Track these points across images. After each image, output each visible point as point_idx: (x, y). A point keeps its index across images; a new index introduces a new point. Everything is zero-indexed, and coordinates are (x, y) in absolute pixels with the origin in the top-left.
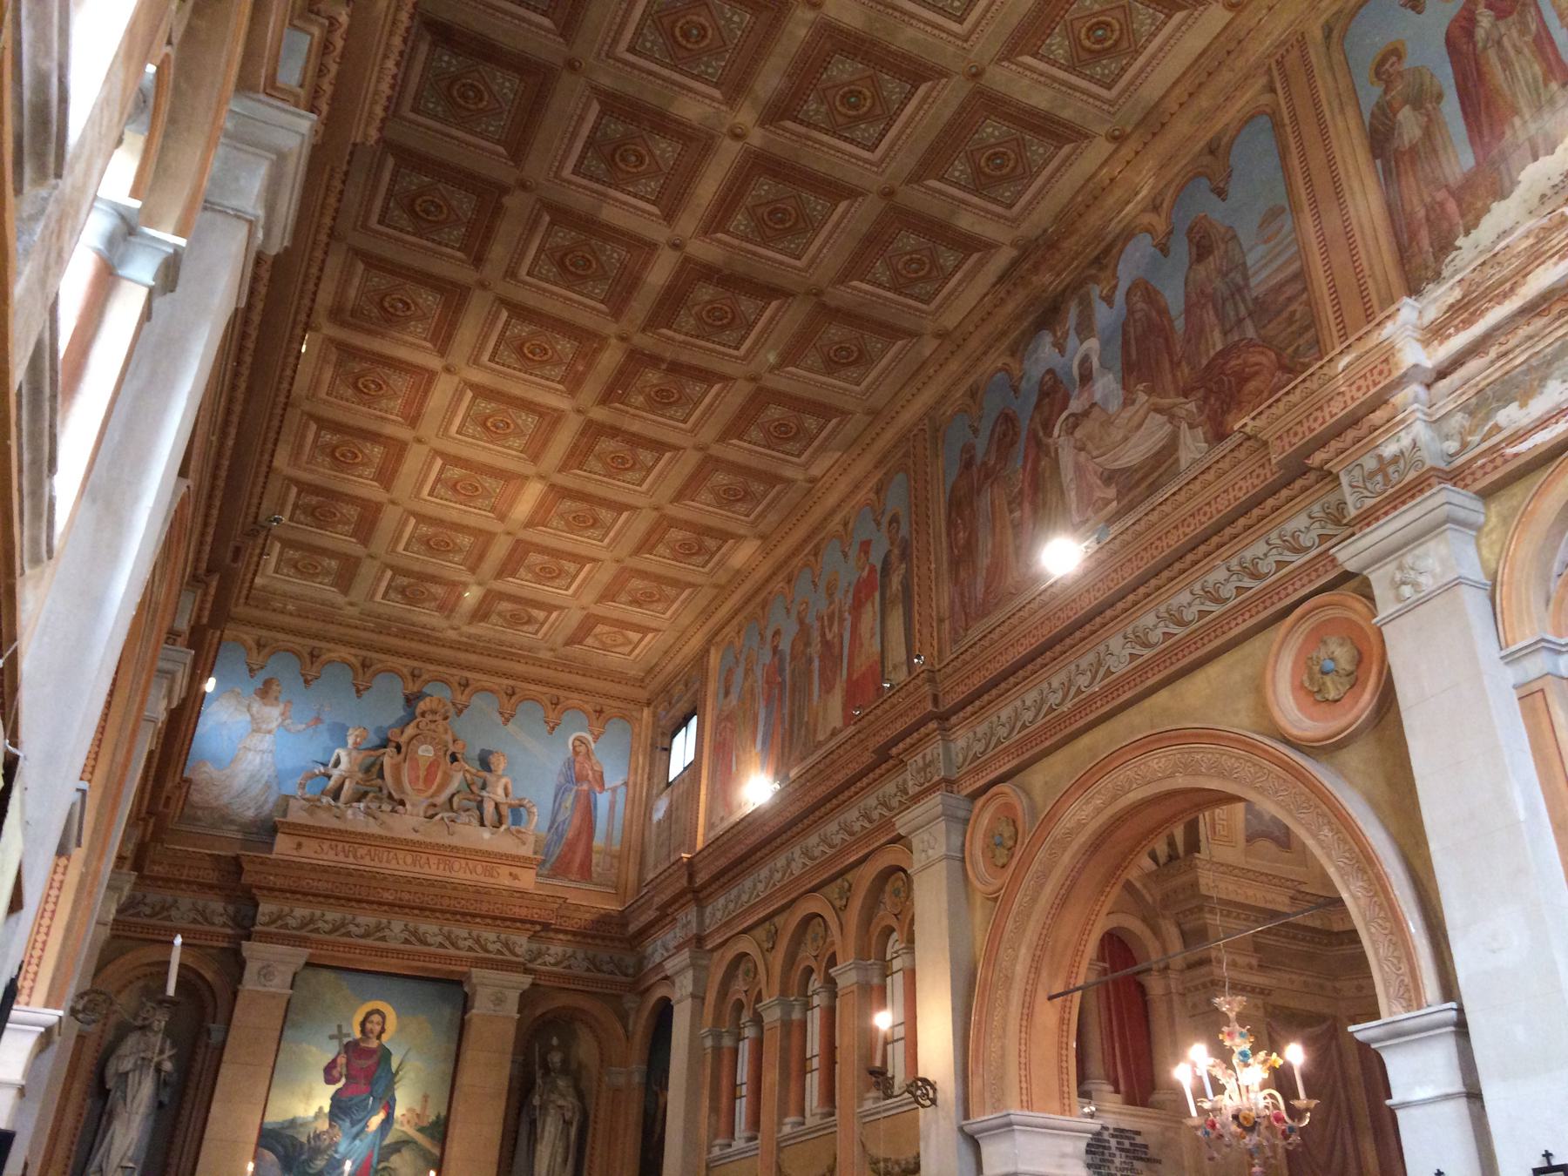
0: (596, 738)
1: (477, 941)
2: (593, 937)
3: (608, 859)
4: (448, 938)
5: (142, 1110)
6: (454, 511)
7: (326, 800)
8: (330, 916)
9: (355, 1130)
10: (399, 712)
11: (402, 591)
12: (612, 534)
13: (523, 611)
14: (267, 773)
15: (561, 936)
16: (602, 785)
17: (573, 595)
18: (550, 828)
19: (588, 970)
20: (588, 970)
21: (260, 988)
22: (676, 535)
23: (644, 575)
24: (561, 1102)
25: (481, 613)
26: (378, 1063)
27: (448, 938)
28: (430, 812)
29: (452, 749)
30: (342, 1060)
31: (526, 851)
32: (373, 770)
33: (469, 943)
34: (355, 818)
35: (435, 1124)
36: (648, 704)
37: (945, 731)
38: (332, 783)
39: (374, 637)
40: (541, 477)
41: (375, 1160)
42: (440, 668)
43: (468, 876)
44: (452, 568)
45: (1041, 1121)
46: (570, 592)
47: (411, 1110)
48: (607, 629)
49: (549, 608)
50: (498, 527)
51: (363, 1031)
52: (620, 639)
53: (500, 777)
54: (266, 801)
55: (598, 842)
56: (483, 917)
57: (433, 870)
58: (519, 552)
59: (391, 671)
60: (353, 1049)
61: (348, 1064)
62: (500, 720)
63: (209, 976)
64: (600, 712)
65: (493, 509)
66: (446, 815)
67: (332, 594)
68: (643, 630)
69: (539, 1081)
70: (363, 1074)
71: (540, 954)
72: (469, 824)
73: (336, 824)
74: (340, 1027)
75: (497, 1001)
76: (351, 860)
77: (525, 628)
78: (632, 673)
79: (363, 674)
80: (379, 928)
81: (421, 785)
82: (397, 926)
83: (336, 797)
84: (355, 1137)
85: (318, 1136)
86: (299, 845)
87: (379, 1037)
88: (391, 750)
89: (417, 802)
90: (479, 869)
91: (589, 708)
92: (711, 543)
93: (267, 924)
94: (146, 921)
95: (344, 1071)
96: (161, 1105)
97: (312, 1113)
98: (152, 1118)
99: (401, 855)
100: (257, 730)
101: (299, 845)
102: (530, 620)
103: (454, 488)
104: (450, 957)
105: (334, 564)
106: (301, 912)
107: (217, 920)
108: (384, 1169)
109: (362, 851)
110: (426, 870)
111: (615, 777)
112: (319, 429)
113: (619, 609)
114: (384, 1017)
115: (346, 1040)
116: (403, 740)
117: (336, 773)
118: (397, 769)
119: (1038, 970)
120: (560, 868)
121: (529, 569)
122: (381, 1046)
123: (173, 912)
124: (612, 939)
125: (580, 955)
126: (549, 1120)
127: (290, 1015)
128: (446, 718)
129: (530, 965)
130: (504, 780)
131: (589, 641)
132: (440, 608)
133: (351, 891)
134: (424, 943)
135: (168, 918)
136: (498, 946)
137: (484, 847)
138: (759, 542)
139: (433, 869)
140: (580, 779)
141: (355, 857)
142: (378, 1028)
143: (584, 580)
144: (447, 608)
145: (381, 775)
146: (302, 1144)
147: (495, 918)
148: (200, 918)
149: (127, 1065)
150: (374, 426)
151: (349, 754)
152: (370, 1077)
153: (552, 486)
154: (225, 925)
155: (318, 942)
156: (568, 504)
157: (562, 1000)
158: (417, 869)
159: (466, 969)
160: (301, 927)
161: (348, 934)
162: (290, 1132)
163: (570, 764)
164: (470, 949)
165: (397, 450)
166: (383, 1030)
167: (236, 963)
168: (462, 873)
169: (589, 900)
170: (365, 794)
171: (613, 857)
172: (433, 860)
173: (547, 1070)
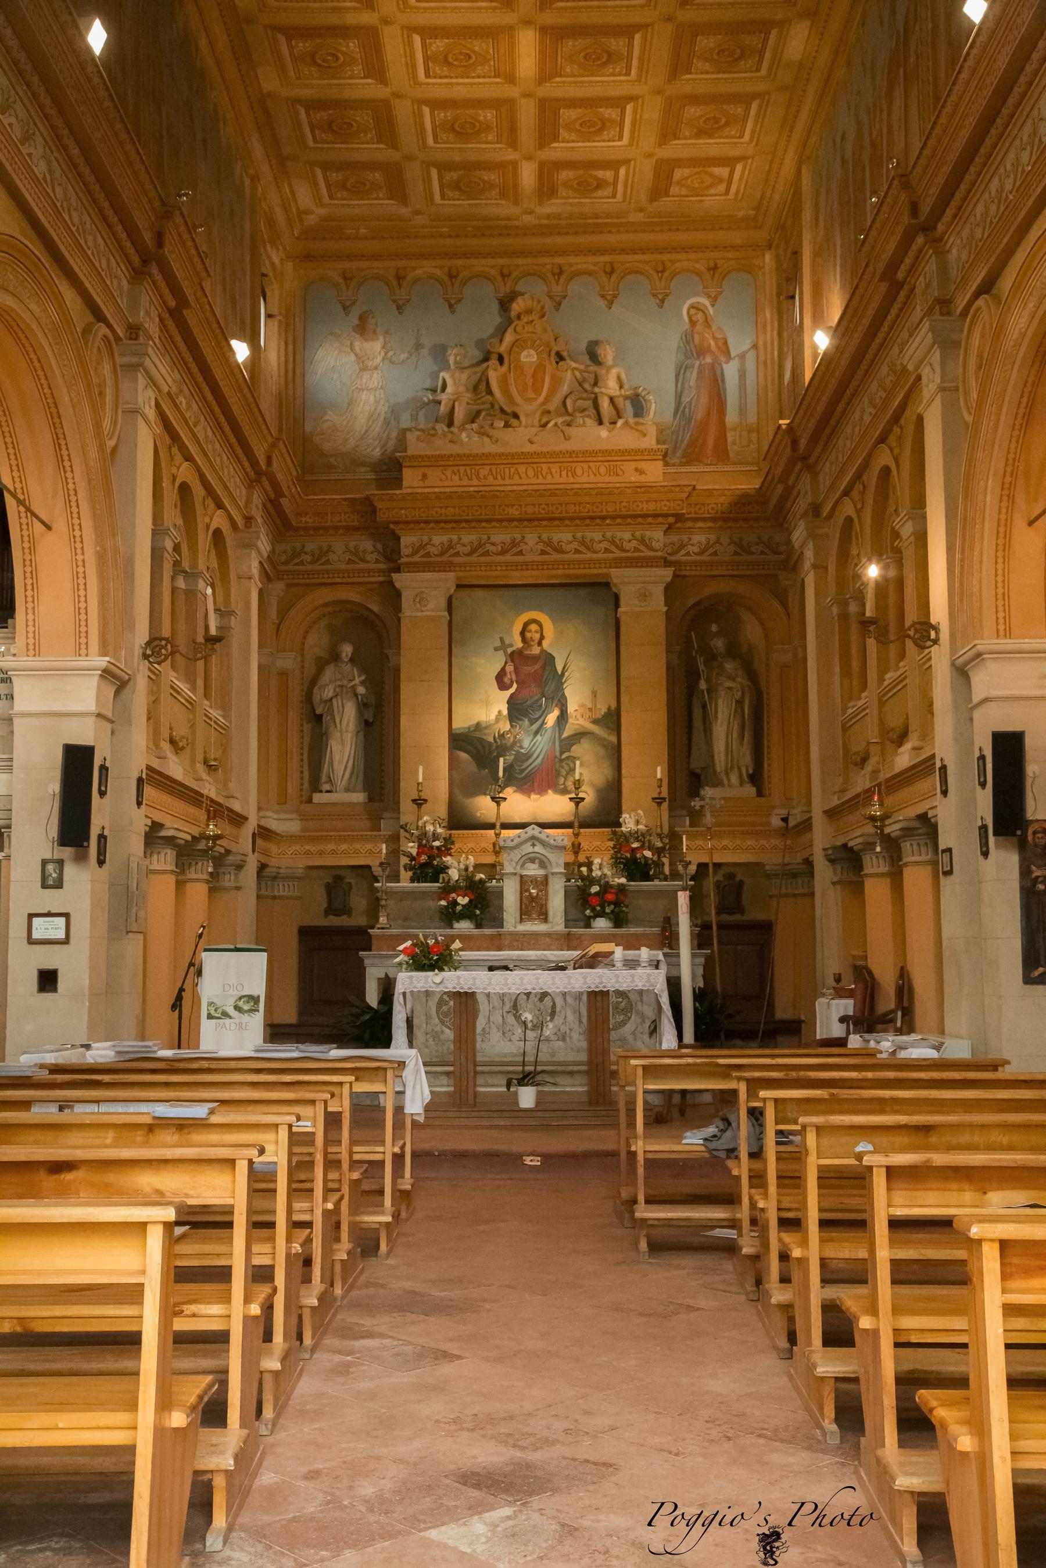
0: (714, 301)
1: (613, 542)
2: (735, 520)
3: (745, 434)
4: (583, 543)
5: (352, 727)
6: (461, 87)
7: (441, 427)
8: (310, 546)
9: (535, 727)
10: (496, 319)
11: (457, 186)
12: (635, 63)
13: (589, 176)
14: (383, 409)
15: (700, 524)
16: (727, 352)
17: (631, 144)
18: (675, 415)
19: (736, 553)
20: (736, 553)
21: (419, 614)
22: (706, 43)
23: (695, 99)
24: (731, 684)
25: (546, 189)
26: (544, 667)
27: (583, 543)
28: (544, 420)
29: (556, 348)
30: (510, 668)
31: (650, 441)
32: (481, 386)
33: (604, 545)
34: (469, 441)
35: (608, 715)
36: (770, 247)
37: (937, 243)
38: (443, 409)
39: (449, 242)
40: (528, 23)
41: (558, 754)
42: (530, 261)
43: (592, 478)
44: (490, 149)
45: (1016, 647)
46: (626, 140)
47: (582, 705)
48: (687, 171)
49: (614, 165)
50: (513, 92)
51: (524, 639)
52: (709, 181)
53: (609, 368)
54: (388, 438)
55: (732, 416)
56: (571, 519)
57: (557, 479)
58: (549, 114)
59: (479, 275)
60: (517, 657)
61: (516, 670)
62: (602, 303)
63: (375, 609)
64: (715, 268)
65: (497, 74)
66: (560, 420)
67: (391, 207)
68: (729, 162)
69: (701, 667)
70: (532, 680)
71: (682, 546)
72: (584, 425)
73: (456, 449)
74: (502, 640)
75: (644, 596)
76: (475, 482)
77: (599, 193)
78: (741, 214)
79: (452, 288)
80: (514, 543)
81: (530, 394)
82: (531, 539)
83: (450, 424)
84: (536, 733)
85: (502, 736)
86: (425, 476)
87: (540, 644)
88: (493, 362)
89: (528, 409)
90: (602, 470)
91: (700, 267)
92: (753, 41)
93: (412, 555)
94: (309, 567)
95: (514, 678)
96: (367, 724)
97: (493, 717)
98: (361, 734)
99: (522, 469)
100: (364, 369)
101: (425, 476)
102: (600, 184)
103: (446, 62)
104: (589, 561)
105: (378, 176)
106: (439, 539)
107: (369, 557)
108: (568, 758)
109: (484, 471)
110: (549, 479)
111: (739, 343)
112: (289, 40)
113: (681, 147)
114: (541, 626)
115: (509, 650)
116: (503, 349)
117: (444, 397)
118: (503, 381)
119: (1011, 499)
120: (692, 455)
121: (569, 128)
122: (543, 651)
123: (331, 556)
124: (756, 520)
125: (725, 540)
126: (720, 701)
127: (455, 635)
128: (542, 316)
129: (669, 558)
130: (614, 372)
131: (674, 190)
132: (503, 194)
133: (475, 514)
134: (559, 551)
135: (328, 562)
136: (634, 543)
137: (604, 446)
138: (807, 23)
139: (556, 477)
140: (701, 352)
141: (478, 478)
142: (537, 636)
143: (633, 123)
144: (510, 192)
145: (489, 392)
146: (490, 744)
147: (624, 517)
148: (354, 558)
149: (328, 693)
150: (333, 20)
151: (452, 376)
152: (538, 679)
153: (544, 30)
154: (377, 561)
155: (460, 565)
156: (570, 44)
157: (712, 588)
158: (541, 480)
159: (605, 571)
160: (443, 553)
161: (487, 553)
162: (477, 734)
163: (688, 338)
164: (607, 551)
165: (371, 37)
166: (542, 638)
167: (393, 596)
168: (586, 477)
169: (726, 482)
170: (478, 413)
171: (750, 431)
172: (555, 468)
173: (711, 658)
